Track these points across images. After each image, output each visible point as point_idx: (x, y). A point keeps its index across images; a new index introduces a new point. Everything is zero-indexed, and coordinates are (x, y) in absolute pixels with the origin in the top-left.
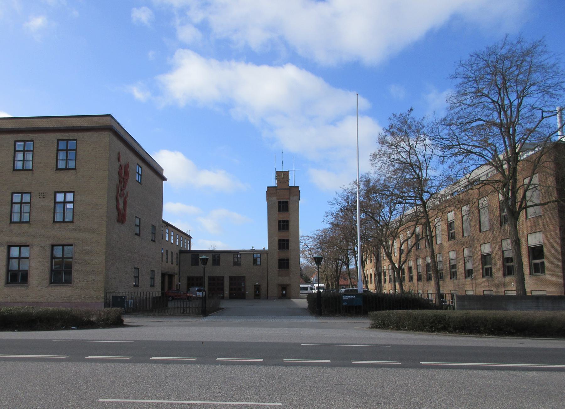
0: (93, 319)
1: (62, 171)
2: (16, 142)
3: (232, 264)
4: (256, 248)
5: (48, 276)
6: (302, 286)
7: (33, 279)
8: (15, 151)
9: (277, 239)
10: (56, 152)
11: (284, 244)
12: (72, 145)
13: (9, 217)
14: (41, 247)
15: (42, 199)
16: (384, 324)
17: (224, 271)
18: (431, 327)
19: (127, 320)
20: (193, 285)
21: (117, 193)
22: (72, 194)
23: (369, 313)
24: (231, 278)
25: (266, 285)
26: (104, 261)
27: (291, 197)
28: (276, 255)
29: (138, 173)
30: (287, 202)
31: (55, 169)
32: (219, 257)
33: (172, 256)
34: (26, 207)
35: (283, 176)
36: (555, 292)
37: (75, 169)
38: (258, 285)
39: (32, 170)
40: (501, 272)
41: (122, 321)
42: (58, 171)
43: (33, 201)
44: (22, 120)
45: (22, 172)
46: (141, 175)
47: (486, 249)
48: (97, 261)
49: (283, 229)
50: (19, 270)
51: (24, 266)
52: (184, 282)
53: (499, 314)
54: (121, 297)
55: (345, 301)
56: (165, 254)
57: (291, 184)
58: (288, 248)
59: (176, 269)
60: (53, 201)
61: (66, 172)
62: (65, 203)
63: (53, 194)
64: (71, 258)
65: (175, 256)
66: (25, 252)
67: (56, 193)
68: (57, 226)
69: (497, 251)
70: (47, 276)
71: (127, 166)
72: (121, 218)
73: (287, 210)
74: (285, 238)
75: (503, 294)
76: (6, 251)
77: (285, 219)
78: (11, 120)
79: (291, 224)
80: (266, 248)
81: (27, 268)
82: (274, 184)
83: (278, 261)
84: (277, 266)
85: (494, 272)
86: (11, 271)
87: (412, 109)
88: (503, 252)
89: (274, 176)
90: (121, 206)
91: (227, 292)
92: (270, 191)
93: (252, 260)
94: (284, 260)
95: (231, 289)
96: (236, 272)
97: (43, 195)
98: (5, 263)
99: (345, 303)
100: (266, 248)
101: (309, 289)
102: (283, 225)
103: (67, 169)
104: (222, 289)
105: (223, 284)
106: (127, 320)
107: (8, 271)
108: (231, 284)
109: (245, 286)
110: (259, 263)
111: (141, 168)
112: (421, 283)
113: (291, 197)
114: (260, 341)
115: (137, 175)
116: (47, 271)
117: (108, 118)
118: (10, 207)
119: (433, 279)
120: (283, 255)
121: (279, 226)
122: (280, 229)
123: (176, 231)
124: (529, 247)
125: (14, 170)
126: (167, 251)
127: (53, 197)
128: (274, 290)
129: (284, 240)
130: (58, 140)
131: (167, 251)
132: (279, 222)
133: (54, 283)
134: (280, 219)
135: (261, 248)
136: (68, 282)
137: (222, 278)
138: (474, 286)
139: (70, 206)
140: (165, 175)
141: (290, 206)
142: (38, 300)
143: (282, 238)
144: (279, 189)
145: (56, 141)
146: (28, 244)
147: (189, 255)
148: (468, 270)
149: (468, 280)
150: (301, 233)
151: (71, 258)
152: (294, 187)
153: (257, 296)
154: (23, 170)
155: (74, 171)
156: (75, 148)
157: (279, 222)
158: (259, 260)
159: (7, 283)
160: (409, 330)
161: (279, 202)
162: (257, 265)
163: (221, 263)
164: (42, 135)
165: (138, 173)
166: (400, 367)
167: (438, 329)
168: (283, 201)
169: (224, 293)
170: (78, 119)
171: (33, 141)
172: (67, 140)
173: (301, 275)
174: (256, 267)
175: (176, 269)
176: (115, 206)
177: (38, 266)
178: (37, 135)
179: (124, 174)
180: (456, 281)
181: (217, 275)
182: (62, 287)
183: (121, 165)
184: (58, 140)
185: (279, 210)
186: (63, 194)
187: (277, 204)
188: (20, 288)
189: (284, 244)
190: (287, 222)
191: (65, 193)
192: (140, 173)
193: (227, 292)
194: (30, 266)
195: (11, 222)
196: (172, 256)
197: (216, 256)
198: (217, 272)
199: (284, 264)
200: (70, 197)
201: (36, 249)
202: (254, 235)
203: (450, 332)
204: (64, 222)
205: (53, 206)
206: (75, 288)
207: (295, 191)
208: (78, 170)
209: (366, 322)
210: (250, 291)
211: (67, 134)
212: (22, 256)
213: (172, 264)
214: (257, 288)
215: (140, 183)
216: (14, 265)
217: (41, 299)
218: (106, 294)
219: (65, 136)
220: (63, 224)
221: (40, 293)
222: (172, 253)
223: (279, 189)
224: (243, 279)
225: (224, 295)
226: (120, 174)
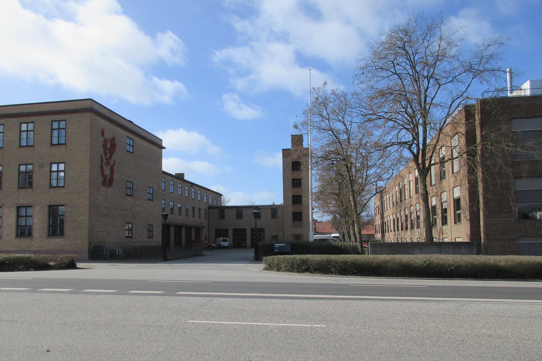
5: (46, 230)
7: (36, 232)
8: (21, 131)
9: (291, 195)
15: (41, 169)
16: (270, 267)
17: (247, 223)
18: (298, 269)
19: (79, 265)
20: (220, 236)
21: (102, 161)
22: (63, 165)
26: (88, 218)
28: (290, 209)
29: (129, 145)
33: (200, 212)
36: (467, 240)
39: (33, 146)
40: (441, 224)
41: (76, 265)
44: (25, 106)
45: (26, 148)
46: (133, 146)
49: (297, 186)
50: (26, 226)
52: (213, 234)
53: (405, 258)
54: (100, 246)
55: (277, 248)
56: (191, 210)
59: (205, 223)
60: (49, 171)
61: (58, 146)
62: (58, 171)
63: (49, 165)
64: (63, 216)
65: (203, 212)
67: (51, 164)
68: (53, 190)
71: (113, 141)
72: (108, 182)
74: (299, 194)
75: (410, 241)
76: (15, 210)
77: (298, 178)
79: (303, 181)
81: (31, 224)
82: (289, 146)
84: (292, 219)
86: (21, 226)
88: (442, 204)
90: (107, 172)
91: (249, 242)
94: (297, 213)
97: (42, 166)
102: (297, 183)
103: (59, 144)
104: (245, 240)
106: (79, 265)
107: (18, 226)
108: (252, 235)
111: (133, 140)
112: (403, 232)
115: (128, 146)
117: (89, 101)
121: (293, 183)
123: (204, 190)
124: (454, 199)
125: (20, 146)
126: (194, 208)
127: (49, 167)
129: (297, 196)
130: (52, 121)
131: (194, 208)
132: (293, 180)
133: (52, 235)
134: (294, 177)
135: (279, 204)
136: (62, 234)
137: (245, 230)
139: (62, 174)
140: (163, 145)
142: (40, 249)
146: (32, 205)
147: (217, 210)
151: (63, 216)
154: (27, 146)
155: (64, 146)
157: (293, 180)
159: (49, 235)
163: (244, 217)
164: (40, 118)
165: (129, 145)
166: (71, 293)
167: (302, 270)
172: (59, 121)
175: (205, 223)
176: (100, 173)
177: (39, 221)
178: (36, 118)
179: (110, 146)
182: (57, 239)
183: (105, 140)
186: (56, 165)
187: (291, 164)
189: (297, 200)
191: (58, 163)
192: (131, 144)
194: (33, 223)
195: (51, 187)
196: (200, 212)
197: (239, 211)
198: (241, 224)
199: (299, 217)
200: (62, 167)
201: (37, 209)
202: (269, 192)
203: (311, 272)
204: (57, 187)
205: (49, 174)
212: (28, 214)
213: (200, 218)
215: (132, 153)
216: (23, 222)
217: (42, 248)
218: (90, 244)
219: (57, 117)
220: (57, 189)
221: (40, 242)
222: (199, 209)
224: (263, 230)
225: (246, 244)
226: (105, 146)
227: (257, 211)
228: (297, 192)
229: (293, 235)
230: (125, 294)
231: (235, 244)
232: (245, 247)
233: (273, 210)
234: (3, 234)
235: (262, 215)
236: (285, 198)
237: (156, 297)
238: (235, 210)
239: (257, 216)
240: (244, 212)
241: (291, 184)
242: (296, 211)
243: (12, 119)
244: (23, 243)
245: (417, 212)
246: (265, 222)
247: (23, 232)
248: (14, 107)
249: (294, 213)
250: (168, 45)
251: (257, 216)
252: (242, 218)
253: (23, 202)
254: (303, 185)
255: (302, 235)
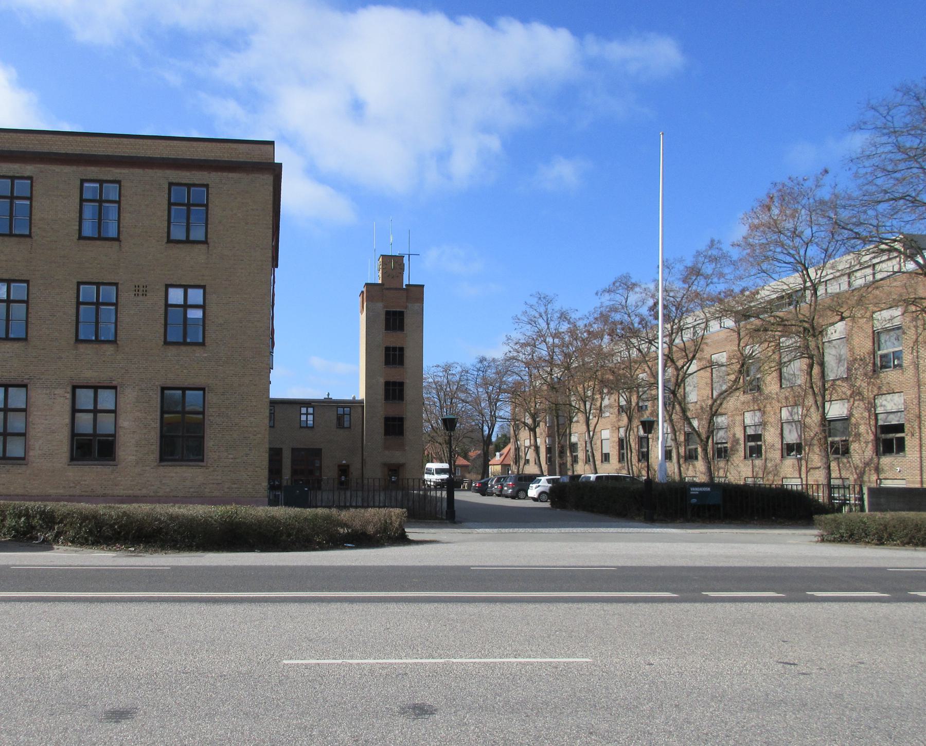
0: (371, 530)
1: (180, 245)
2: (83, 181)
4: (335, 396)
7: (127, 451)
9: (382, 381)
10: (166, 207)
11: (394, 391)
12: (21, 187)
13: (74, 330)
14: (141, 390)
15: (140, 298)
19: (412, 533)
23: (816, 517)
27: (409, 305)
28: (381, 410)
30: (401, 314)
31: (165, 240)
34: (107, 312)
35: (393, 265)
38: (344, 465)
42: (81, 242)
43: (122, 301)
45: (99, 243)
47: (836, 410)
48: (252, 419)
49: (394, 363)
51: (106, 424)
55: (695, 496)
58: (401, 398)
62: (186, 306)
66: (106, 400)
67: (168, 286)
68: (173, 350)
69: (860, 413)
70: (153, 447)
73: (401, 328)
74: (397, 379)
76: (69, 396)
78: (71, 138)
79: (408, 354)
80: (361, 395)
82: (377, 278)
83: (383, 421)
84: (382, 431)
85: (854, 447)
87: (826, 172)
92: (372, 292)
94: (394, 419)
97: (141, 291)
98: (67, 420)
99: (694, 501)
100: (361, 395)
102: (395, 355)
107: (73, 434)
108: (294, 461)
109: (320, 468)
110: (346, 424)
113: (409, 305)
114: (860, 565)
116: (154, 436)
118: (74, 311)
119: (699, 458)
120: (394, 411)
121: (387, 356)
125: (81, 237)
129: (394, 383)
130: (171, 184)
138: (804, 469)
141: (408, 320)
143: (392, 379)
145: (166, 186)
146: (114, 383)
148: (788, 445)
149: (790, 461)
153: (343, 485)
155: (203, 247)
156: (29, 195)
157: (387, 349)
158: (347, 418)
159: (72, 459)
160: (904, 544)
162: (343, 427)
170: (209, 145)
171: (119, 182)
177: (136, 427)
178: (125, 171)
180: (758, 462)
182: (184, 469)
184: (171, 184)
187: (383, 317)
188: (99, 468)
191: (186, 287)
199: (394, 427)
200: (196, 296)
205: (162, 311)
206: (211, 469)
207: (416, 293)
208: (211, 244)
209: (812, 533)
210: (329, 472)
211: (188, 174)
214: (344, 470)
216: (85, 422)
219: (93, 171)
220: (184, 348)
221: (138, 478)
224: (317, 453)
228: (394, 374)
229: (385, 465)
230: (694, 600)
234: (31, 453)
237: (660, 606)
242: (392, 414)
243: (57, 168)
244: (91, 475)
245: (745, 428)
247: (93, 448)
248: (63, 138)
249: (387, 420)
253: (90, 375)
254: (407, 361)
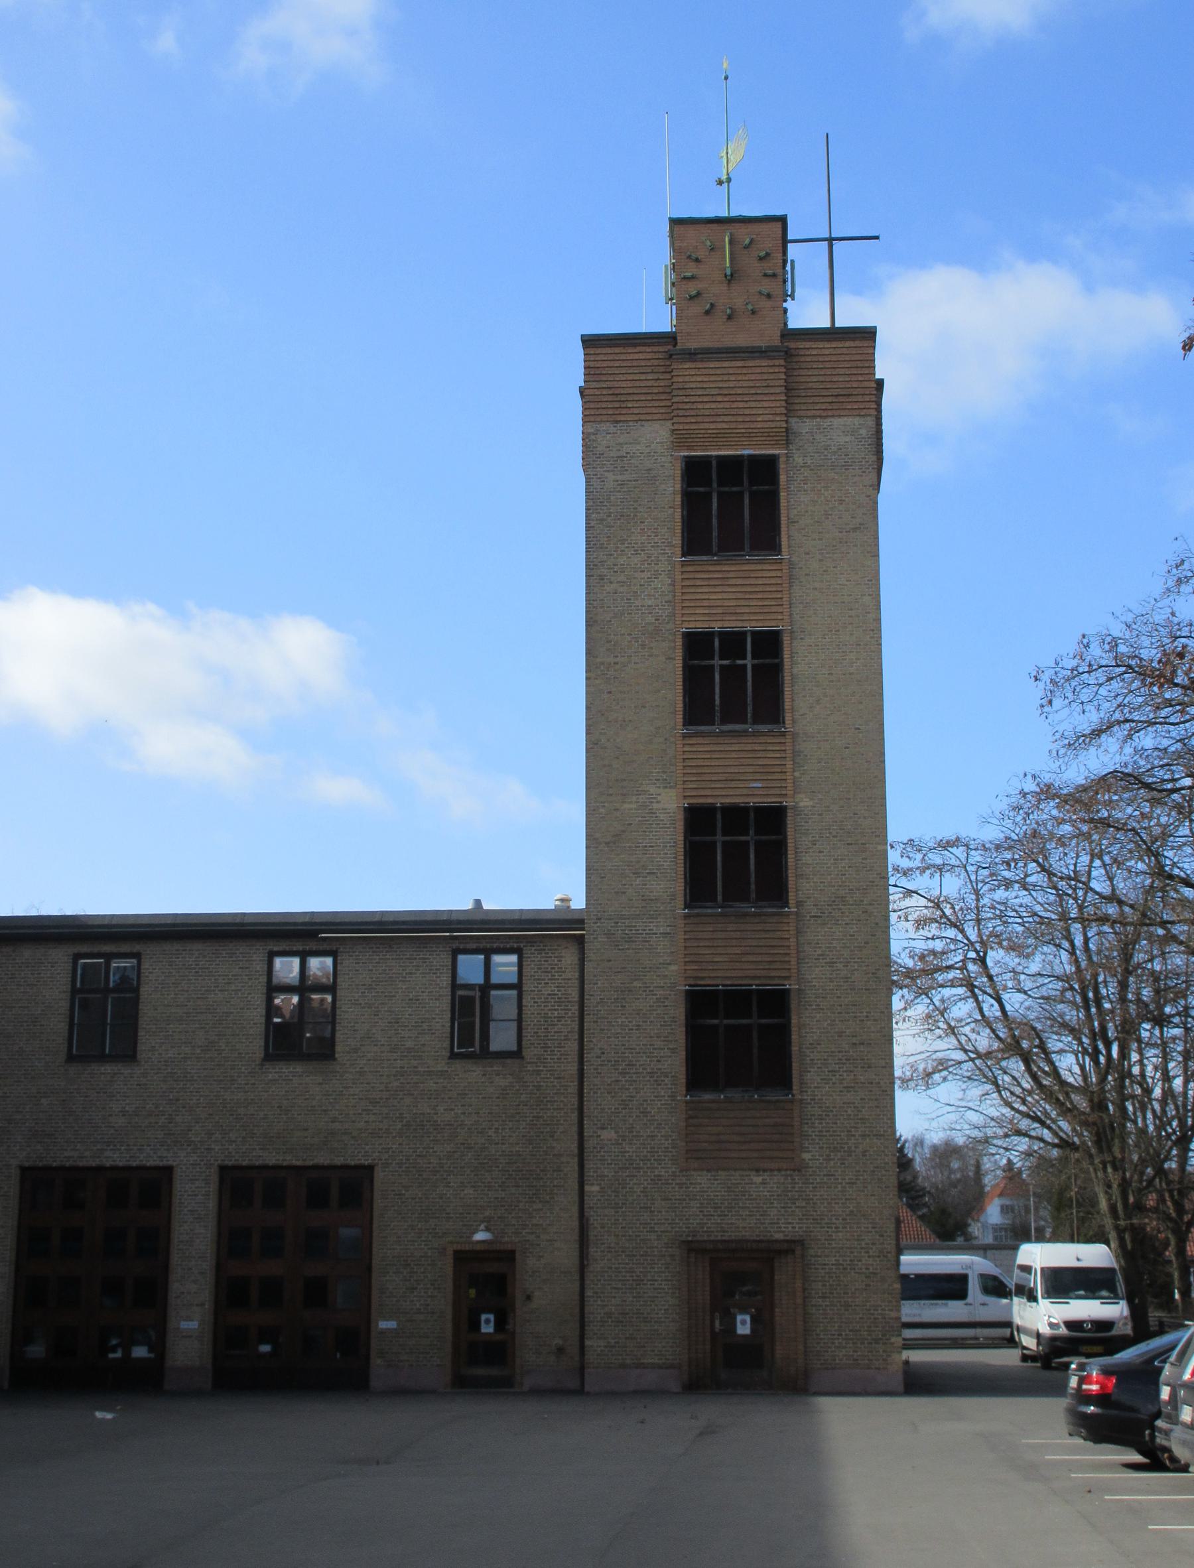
3: (256, 1046)
6: (914, 1262)
9: (670, 804)
11: (737, 856)
17: (189, 1114)
24: (236, 1184)
25: (564, 1254)
27: (804, 427)
28: (665, 956)
30: (764, 472)
32: (128, 993)
35: (731, 258)
37: (517, 1054)
57: (807, 311)
74: (750, 791)
77: (752, 623)
79: (803, 664)
80: (579, 902)
83: (679, 1012)
84: (675, 1064)
89: (658, 256)
91: (190, 1322)
92: (617, 371)
93: (443, 1005)
94: (737, 1000)
95: (231, 1293)
96: (299, 1119)
100: (579, 902)
101: (974, 1287)
102: (733, 675)
104: (152, 1293)
105: (155, 1244)
108: (232, 1242)
110: (502, 1038)
113: (804, 427)
120: (735, 954)
121: (695, 681)
122: (697, 711)
128: (646, 1306)
129: (736, 816)
134: (699, 624)
137: (154, 1186)
141: (798, 502)
143: (722, 795)
144: (691, 355)
150: (898, 828)
152: (833, 334)
158: (503, 1005)
161: (696, 472)
163: (147, 1041)
168: (729, 468)
169: (162, 1332)
173: (909, 1190)
174: (472, 1074)
181: (115, 1157)
185: (696, 541)
187: (671, 488)
189: (737, 856)
190: (769, 644)
193: (190, 1322)
199: (744, 1044)
210: (409, 1304)
214: (487, 1278)
223: (691, 355)
224: (350, 1187)
225: (159, 1347)
227: (295, 978)
228: (735, 771)
231: (37, 1350)
232: (146, 1382)
233: (454, 957)
235: (355, 1021)
236: (604, 840)
238: (59, 958)
239: (299, 1039)
240: (160, 978)
241: (673, 694)
246: (372, 1098)
249: (701, 1003)
250: (970, 1221)
251: (299, 1039)
252: (127, 1053)
255: (791, 1248)
